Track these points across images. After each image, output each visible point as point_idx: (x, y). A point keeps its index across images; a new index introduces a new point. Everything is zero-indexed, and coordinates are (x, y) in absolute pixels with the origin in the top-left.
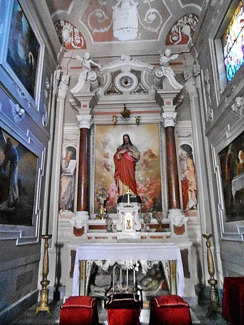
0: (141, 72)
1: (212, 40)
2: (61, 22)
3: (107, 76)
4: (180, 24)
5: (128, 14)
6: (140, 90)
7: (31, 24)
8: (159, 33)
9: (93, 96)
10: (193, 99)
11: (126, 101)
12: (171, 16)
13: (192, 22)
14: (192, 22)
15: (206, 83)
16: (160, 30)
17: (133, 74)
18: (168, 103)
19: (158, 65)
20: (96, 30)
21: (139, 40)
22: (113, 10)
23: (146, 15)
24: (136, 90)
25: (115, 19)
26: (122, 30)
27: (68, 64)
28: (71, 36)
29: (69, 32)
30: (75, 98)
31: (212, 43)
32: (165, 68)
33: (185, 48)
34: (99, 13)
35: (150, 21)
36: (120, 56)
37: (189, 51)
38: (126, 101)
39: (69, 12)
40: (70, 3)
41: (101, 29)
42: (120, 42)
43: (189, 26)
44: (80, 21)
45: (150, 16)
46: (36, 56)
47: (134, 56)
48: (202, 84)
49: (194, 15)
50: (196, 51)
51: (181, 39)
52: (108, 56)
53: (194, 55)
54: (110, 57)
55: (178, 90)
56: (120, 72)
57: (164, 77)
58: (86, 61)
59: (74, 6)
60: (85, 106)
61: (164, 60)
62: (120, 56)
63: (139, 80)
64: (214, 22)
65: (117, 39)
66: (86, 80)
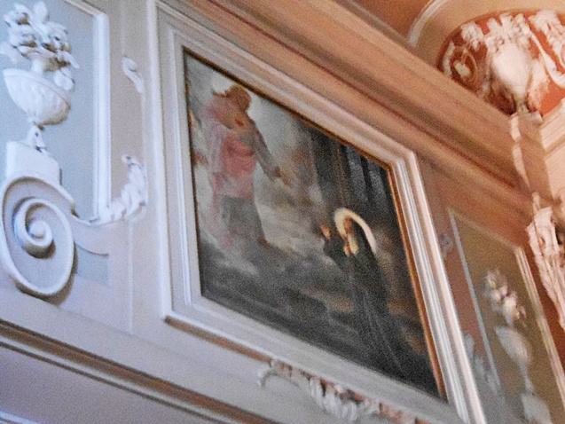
2: (464, 35)
28: (536, 55)
46: (387, 217)
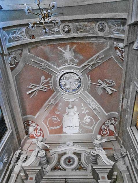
0: (81, 154)
1: (129, 128)
3: (55, 157)
4: (107, 124)
5: (73, 119)
6: (80, 168)
7: (4, 115)
8: (93, 129)
9: (40, 170)
10: (126, 177)
11: (67, 176)
12: (100, 120)
13: (114, 123)
14: (114, 123)
15: (133, 161)
16: (93, 128)
17: (75, 155)
18: (103, 178)
19: (93, 148)
20: (51, 128)
21: (80, 133)
22: (63, 117)
23: (84, 119)
24: (77, 168)
25: (64, 121)
26: (68, 127)
27: (28, 147)
28: (35, 131)
29: (34, 128)
30: (25, 172)
31: (130, 130)
32: (98, 149)
33: (113, 138)
34: (55, 118)
35: (87, 123)
36: (66, 143)
37: (115, 140)
38: (67, 176)
39: (36, 117)
40: (38, 111)
41: (55, 127)
42: (67, 135)
43: (113, 125)
44: (42, 122)
45: (87, 120)
47: (76, 143)
48: (130, 161)
49: (114, 118)
50: (121, 140)
51: (108, 133)
52: (57, 142)
53: (119, 142)
54: (60, 143)
55: (110, 165)
56: (65, 153)
57: (98, 155)
58: (39, 142)
59: (40, 114)
60: (31, 179)
61: (96, 142)
62: (66, 143)
63: (80, 160)
64: (127, 117)
65: (65, 133)
66: (37, 156)
